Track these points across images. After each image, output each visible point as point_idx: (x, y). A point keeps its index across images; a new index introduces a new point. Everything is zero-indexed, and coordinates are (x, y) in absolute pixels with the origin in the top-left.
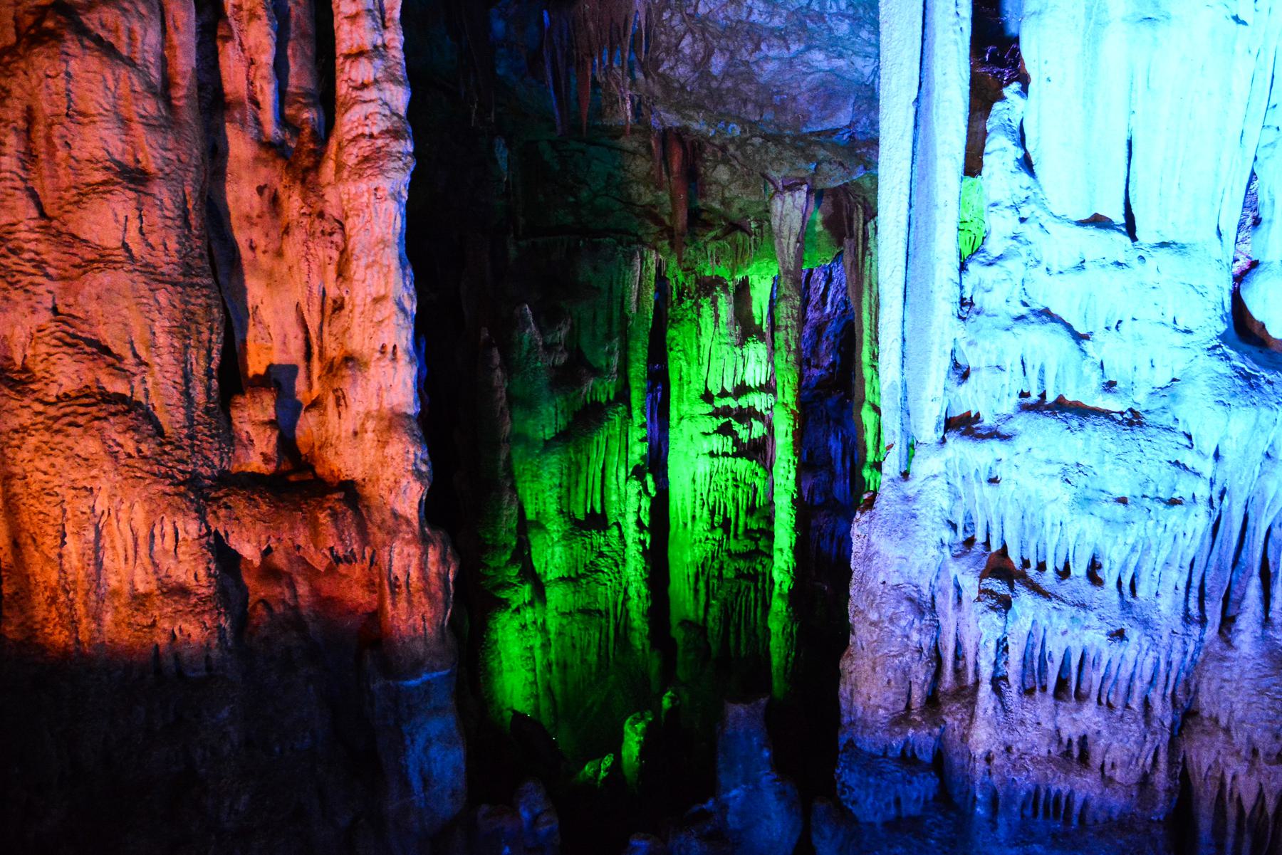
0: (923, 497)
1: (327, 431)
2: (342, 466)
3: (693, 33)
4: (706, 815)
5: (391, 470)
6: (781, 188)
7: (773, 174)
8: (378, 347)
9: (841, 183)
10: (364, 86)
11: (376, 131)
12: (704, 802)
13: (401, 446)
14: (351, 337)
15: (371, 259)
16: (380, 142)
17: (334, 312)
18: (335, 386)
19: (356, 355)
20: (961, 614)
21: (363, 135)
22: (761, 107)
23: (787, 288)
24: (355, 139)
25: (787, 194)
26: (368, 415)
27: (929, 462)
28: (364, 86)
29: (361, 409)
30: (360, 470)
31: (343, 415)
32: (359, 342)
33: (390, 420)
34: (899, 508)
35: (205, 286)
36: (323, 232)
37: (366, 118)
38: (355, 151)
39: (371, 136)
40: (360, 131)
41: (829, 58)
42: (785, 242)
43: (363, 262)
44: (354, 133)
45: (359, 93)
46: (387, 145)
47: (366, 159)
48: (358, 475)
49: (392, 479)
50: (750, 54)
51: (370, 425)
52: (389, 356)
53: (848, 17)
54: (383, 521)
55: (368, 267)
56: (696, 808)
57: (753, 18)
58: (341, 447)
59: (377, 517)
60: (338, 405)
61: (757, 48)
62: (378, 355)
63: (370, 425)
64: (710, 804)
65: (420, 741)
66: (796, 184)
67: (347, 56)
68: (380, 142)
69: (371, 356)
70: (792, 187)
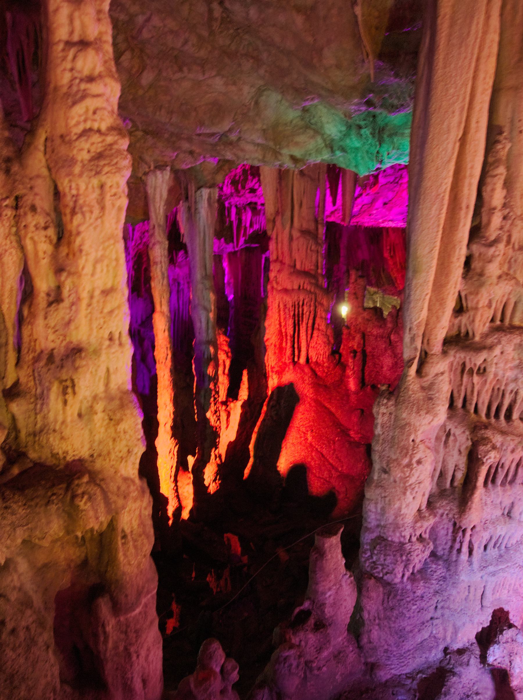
0: (436, 387)
1: (45, 417)
2: (69, 448)
3: (133, 50)
4: (307, 614)
5: (124, 442)
6: (152, 168)
7: (147, 158)
8: (106, 336)
9: (190, 166)
10: (91, 79)
11: (104, 127)
12: (301, 604)
13: (133, 420)
14: (77, 328)
15: (100, 254)
16: (109, 139)
17: (50, 304)
18: (64, 377)
19: (83, 345)
20: (447, 450)
21: (91, 130)
22: (171, 112)
23: (160, 236)
24: (86, 132)
25: (158, 173)
26: (95, 398)
27: (439, 366)
28: (91, 79)
29: (88, 393)
30: (87, 447)
31: (70, 402)
32: (82, 333)
33: (121, 399)
34: (420, 395)
35: (208, 334)
36: (36, 226)
37: (94, 113)
38: (87, 146)
39: (99, 131)
40: (88, 125)
41: (226, 84)
42: (157, 205)
43: (92, 258)
44: (81, 128)
45: (88, 86)
46: (115, 143)
47: (100, 156)
48: (84, 453)
49: (125, 450)
50: (174, 74)
51: (99, 407)
52: (117, 342)
53: (253, 58)
54: (119, 488)
55: (97, 262)
56: (297, 610)
57: (186, 48)
58: (67, 432)
59: (113, 487)
60: (64, 392)
61: (181, 70)
62: (107, 343)
63: (99, 407)
64: (307, 605)
65: (143, 653)
66: (163, 166)
67: (69, 44)
68: (109, 139)
69: (101, 344)
70: (160, 167)
